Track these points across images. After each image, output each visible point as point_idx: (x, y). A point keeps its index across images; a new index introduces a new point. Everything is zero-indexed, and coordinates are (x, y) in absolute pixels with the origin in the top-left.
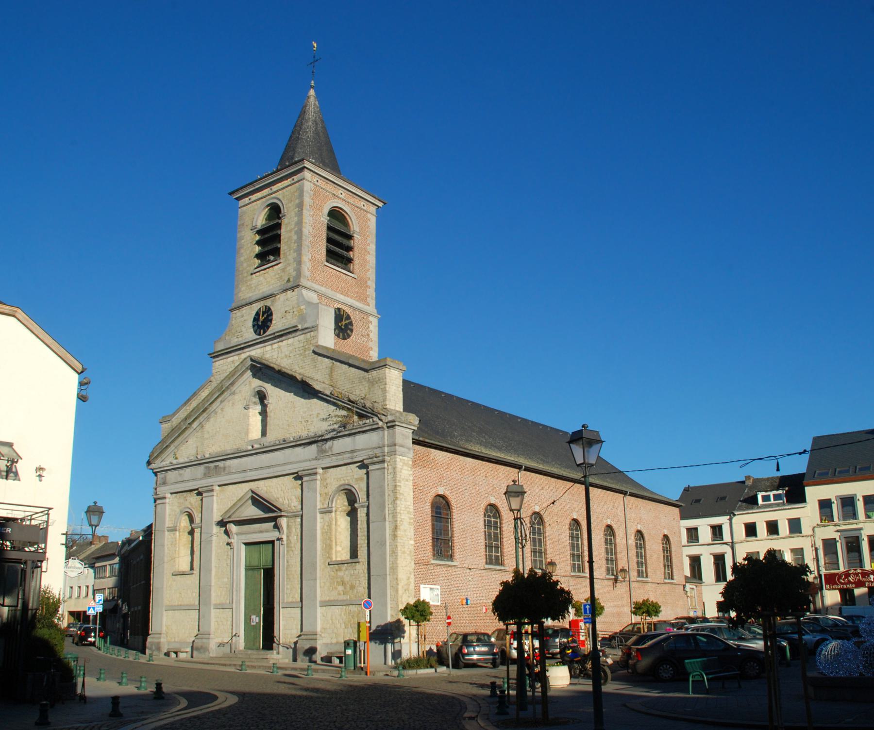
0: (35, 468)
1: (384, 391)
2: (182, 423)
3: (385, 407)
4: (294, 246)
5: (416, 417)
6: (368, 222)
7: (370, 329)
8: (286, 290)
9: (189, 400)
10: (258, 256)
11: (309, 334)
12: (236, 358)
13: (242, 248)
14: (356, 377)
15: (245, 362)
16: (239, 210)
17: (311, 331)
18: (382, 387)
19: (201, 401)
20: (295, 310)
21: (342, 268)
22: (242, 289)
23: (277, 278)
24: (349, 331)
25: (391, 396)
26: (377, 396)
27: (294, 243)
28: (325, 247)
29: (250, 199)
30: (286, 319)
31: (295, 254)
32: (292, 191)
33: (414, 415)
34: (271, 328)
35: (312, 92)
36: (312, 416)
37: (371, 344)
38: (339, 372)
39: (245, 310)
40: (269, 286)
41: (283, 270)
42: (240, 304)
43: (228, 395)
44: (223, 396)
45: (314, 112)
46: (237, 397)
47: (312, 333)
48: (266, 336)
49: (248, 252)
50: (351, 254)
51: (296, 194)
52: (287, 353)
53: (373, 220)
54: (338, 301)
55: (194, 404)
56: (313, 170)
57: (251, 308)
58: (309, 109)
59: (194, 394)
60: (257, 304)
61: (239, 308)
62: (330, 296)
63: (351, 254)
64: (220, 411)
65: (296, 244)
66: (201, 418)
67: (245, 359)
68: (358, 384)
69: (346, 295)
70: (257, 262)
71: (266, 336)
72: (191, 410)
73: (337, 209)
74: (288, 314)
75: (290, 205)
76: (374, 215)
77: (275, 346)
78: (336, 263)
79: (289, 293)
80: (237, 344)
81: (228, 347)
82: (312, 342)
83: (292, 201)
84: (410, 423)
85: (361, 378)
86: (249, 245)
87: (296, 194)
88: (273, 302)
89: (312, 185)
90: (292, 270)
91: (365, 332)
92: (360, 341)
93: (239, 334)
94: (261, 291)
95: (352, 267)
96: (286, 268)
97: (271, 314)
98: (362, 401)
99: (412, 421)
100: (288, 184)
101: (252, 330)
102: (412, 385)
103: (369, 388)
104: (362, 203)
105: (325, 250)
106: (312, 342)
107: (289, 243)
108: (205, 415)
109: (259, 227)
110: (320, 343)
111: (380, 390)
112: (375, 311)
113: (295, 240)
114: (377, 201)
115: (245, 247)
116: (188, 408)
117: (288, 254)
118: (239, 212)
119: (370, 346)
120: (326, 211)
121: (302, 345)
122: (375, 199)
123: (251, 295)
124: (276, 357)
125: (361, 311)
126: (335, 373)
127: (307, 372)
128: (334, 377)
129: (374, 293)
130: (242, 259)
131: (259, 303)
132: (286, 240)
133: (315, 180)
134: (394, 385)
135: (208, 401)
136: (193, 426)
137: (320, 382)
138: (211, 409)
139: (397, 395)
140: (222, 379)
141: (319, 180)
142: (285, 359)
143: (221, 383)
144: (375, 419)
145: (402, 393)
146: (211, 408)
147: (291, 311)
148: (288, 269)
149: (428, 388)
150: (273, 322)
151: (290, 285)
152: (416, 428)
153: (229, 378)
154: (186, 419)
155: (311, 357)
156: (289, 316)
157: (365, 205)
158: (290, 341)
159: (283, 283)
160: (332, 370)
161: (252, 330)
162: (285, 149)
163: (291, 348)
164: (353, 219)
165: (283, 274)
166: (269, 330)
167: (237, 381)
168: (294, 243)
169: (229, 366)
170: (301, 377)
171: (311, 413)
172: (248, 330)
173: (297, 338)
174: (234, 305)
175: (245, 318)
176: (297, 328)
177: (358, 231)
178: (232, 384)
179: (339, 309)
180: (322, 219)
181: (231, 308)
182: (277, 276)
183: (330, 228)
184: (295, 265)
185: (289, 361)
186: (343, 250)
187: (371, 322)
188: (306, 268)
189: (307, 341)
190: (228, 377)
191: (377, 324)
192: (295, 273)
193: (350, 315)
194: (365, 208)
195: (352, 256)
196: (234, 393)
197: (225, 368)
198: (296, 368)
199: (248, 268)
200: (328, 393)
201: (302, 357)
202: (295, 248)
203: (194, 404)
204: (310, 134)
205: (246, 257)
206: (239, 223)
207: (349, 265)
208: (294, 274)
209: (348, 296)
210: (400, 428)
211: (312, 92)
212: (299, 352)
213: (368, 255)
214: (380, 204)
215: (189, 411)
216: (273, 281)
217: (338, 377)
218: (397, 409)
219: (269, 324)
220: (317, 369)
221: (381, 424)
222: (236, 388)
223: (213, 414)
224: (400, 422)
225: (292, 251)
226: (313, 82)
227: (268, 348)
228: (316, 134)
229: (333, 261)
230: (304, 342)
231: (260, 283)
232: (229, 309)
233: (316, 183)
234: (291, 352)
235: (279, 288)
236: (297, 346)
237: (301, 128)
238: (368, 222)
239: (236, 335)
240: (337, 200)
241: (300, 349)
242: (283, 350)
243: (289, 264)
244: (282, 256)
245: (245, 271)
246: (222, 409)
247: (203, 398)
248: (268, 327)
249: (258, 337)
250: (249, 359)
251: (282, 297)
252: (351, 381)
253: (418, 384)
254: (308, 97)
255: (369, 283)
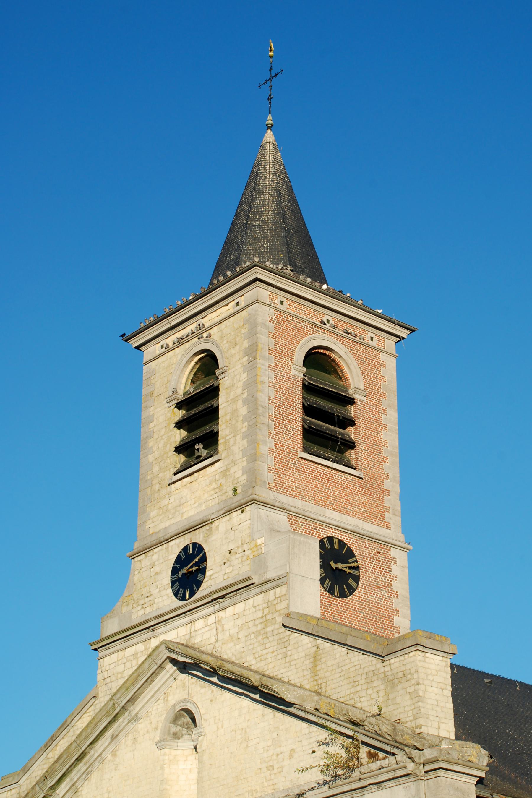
0: (156, 572)
1: (416, 697)
2: (37, 788)
3: (418, 731)
4: (243, 427)
5: (483, 751)
6: (382, 368)
7: (392, 573)
8: (229, 511)
9: (53, 739)
10: (179, 450)
11: (272, 592)
12: (140, 647)
13: (152, 437)
14: (361, 671)
15: (156, 653)
16: (144, 367)
17: (278, 586)
18: (411, 690)
19: (74, 738)
20: (246, 547)
21: (334, 461)
22: (152, 514)
23: (214, 489)
24: (351, 581)
25: (429, 707)
26: (401, 710)
27: (243, 421)
28: (300, 424)
29: (237, 304)
30: (231, 565)
31: (245, 441)
32: (236, 326)
33: (477, 746)
34: (204, 586)
35: (269, 137)
36: (281, 756)
37: (395, 603)
38: (329, 664)
39: (157, 554)
40: (200, 505)
41: (224, 473)
42: (148, 542)
43: (126, 721)
44: (116, 726)
45: (275, 174)
46: (142, 726)
47: (278, 590)
48: (195, 601)
49: (161, 445)
50: (351, 432)
51: (243, 331)
52: (233, 631)
53: (391, 363)
54: (329, 525)
55: (62, 744)
56: (274, 283)
57: (167, 549)
58: (265, 168)
59: (64, 726)
60: (178, 541)
61: (145, 550)
62: (312, 516)
63: (351, 432)
64: (110, 757)
65: (246, 424)
66: (74, 775)
67: (157, 648)
68: (364, 687)
69: (344, 511)
70: (182, 458)
71: (195, 601)
72: (56, 757)
73: (321, 351)
74: (233, 557)
75: (233, 351)
76: (391, 355)
77: (212, 619)
78: (321, 451)
79: (236, 516)
80: (143, 620)
81: (126, 627)
82: (279, 607)
83: (236, 344)
84: (469, 764)
85: (371, 674)
86: (163, 432)
87: (243, 331)
88: (208, 536)
89: (272, 310)
90: (240, 473)
91: (383, 580)
92: (375, 598)
93: (147, 600)
94: (185, 517)
95: (353, 456)
96: (228, 470)
97: (204, 559)
98: (373, 720)
99: (474, 760)
100: (229, 313)
101: (170, 591)
102: (486, 681)
103: (387, 694)
104: (369, 335)
105: (300, 428)
106: (279, 607)
107: (234, 422)
108: (81, 767)
109: (180, 396)
110: (293, 609)
111: (408, 697)
112: (402, 537)
113: (244, 417)
114: (397, 327)
115: (156, 436)
116: (50, 755)
117: (232, 442)
118: (144, 371)
119: (394, 607)
120: (299, 356)
121: (260, 614)
122: (392, 325)
123: (167, 524)
124: (213, 640)
125: (373, 540)
126: (323, 666)
127: (271, 666)
128: (321, 674)
129: (399, 503)
130: (151, 458)
131: (182, 539)
132: (228, 417)
133: (278, 301)
134: (434, 684)
135: (86, 738)
136: (58, 792)
137: (294, 685)
138: (93, 753)
139: (441, 704)
140: (114, 690)
141: (284, 300)
142: (231, 645)
143: (111, 699)
144: (400, 756)
145: (451, 700)
146: (92, 752)
147: (240, 550)
148: (232, 471)
149: (521, 684)
150: (208, 573)
151: (238, 499)
152: (483, 775)
153: (127, 689)
154: (45, 777)
155: (276, 637)
156: (235, 560)
157: (375, 338)
158: (240, 607)
159: (224, 498)
160: (316, 658)
161: (170, 590)
162: (224, 248)
163: (239, 622)
164: (351, 367)
165: (223, 481)
166: (201, 589)
167: (141, 693)
168: (243, 421)
169: (128, 665)
170: (258, 677)
171: (279, 750)
172: (163, 593)
173: (251, 601)
174: (137, 546)
175: (157, 569)
176: (251, 582)
177: (362, 387)
178: (132, 700)
179: (330, 539)
180: (293, 372)
181: (131, 553)
182: (214, 485)
183: (308, 388)
184: (245, 463)
185: (238, 647)
186: (335, 426)
187: (394, 560)
188: (266, 467)
189: (270, 605)
190: (125, 687)
191: (406, 563)
192: (245, 477)
193: (353, 548)
194: (374, 343)
195: (352, 436)
196: (135, 719)
197: (121, 668)
198: (251, 661)
199: (161, 475)
200: (310, 707)
201: (260, 638)
202: (244, 430)
203: (62, 744)
204: (268, 216)
205: (157, 454)
206: (144, 392)
207: (347, 453)
208: (243, 479)
209: (347, 514)
210: (450, 774)
211: (269, 137)
212: (254, 629)
213: (384, 432)
214: (404, 333)
215: (52, 761)
216: (206, 495)
217: (327, 674)
218: (443, 734)
219: (200, 576)
220: (288, 659)
221: (411, 766)
222: (141, 705)
223: (96, 763)
224: (447, 761)
225: (238, 437)
226: (270, 117)
227: (199, 624)
228: (278, 214)
229: (316, 449)
230: (263, 609)
231: (183, 501)
232: (128, 554)
233: (279, 306)
234: (241, 629)
235: (217, 508)
236: (251, 618)
237: (250, 207)
238: (382, 368)
239: (141, 602)
240: (319, 335)
241: (257, 622)
242: (226, 627)
243: (234, 462)
244: (221, 447)
245: (156, 481)
246: (114, 754)
247: (78, 732)
248: (199, 584)
249: (181, 603)
250: (163, 648)
251: (222, 524)
252: (351, 680)
253: (499, 678)
254: (263, 147)
255: (388, 484)
